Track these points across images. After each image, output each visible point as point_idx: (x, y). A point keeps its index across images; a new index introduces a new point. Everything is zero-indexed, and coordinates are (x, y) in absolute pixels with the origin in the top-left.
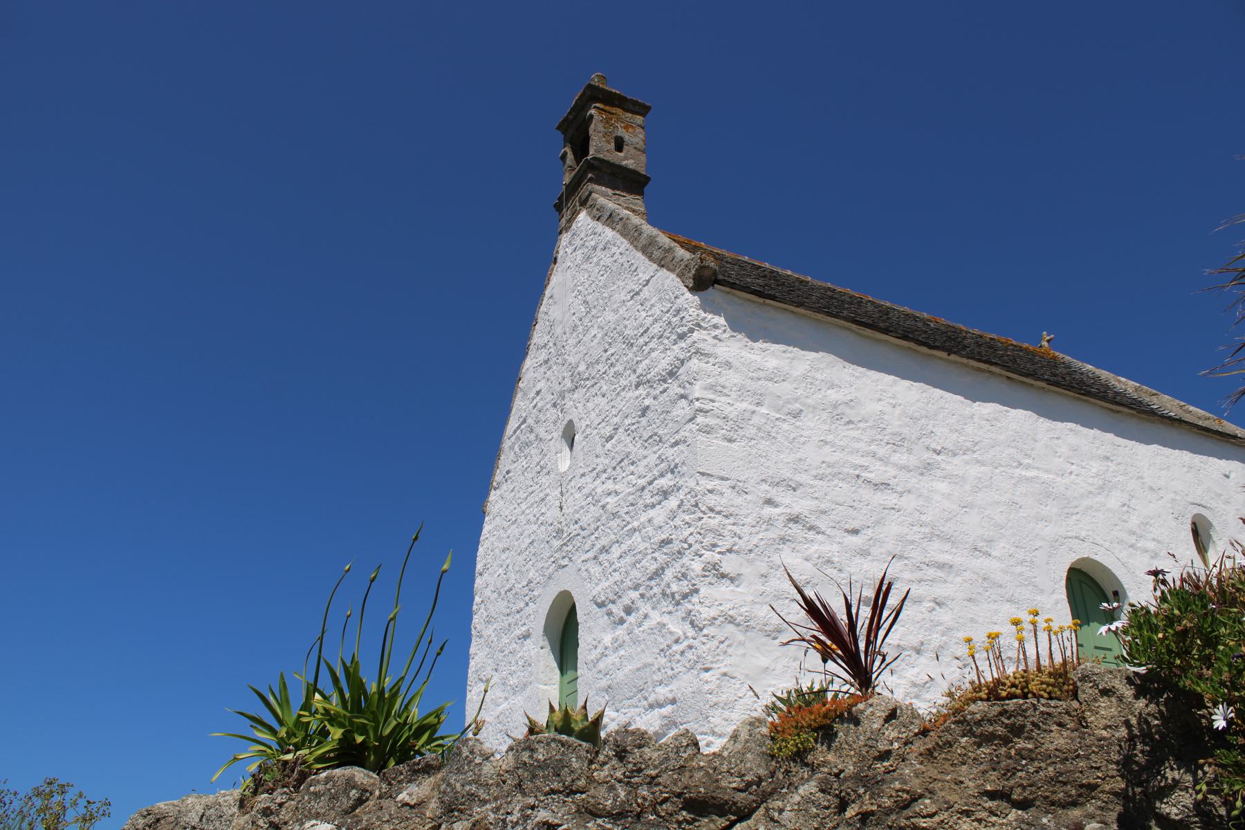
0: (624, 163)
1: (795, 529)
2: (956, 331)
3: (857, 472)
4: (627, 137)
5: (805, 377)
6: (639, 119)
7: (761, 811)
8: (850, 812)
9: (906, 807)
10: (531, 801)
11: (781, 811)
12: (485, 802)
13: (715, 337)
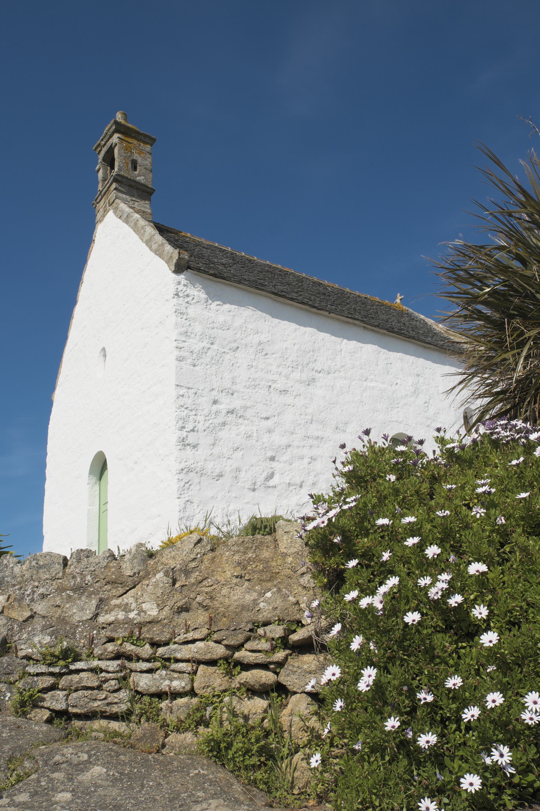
0: (138, 178)
1: (231, 418)
2: (343, 293)
3: (270, 384)
4: (139, 160)
5: (241, 327)
6: (148, 148)
7: (140, 585)
8: (177, 585)
9: (200, 582)
10: (36, 584)
11: (148, 585)
12: (14, 585)
13: (187, 302)
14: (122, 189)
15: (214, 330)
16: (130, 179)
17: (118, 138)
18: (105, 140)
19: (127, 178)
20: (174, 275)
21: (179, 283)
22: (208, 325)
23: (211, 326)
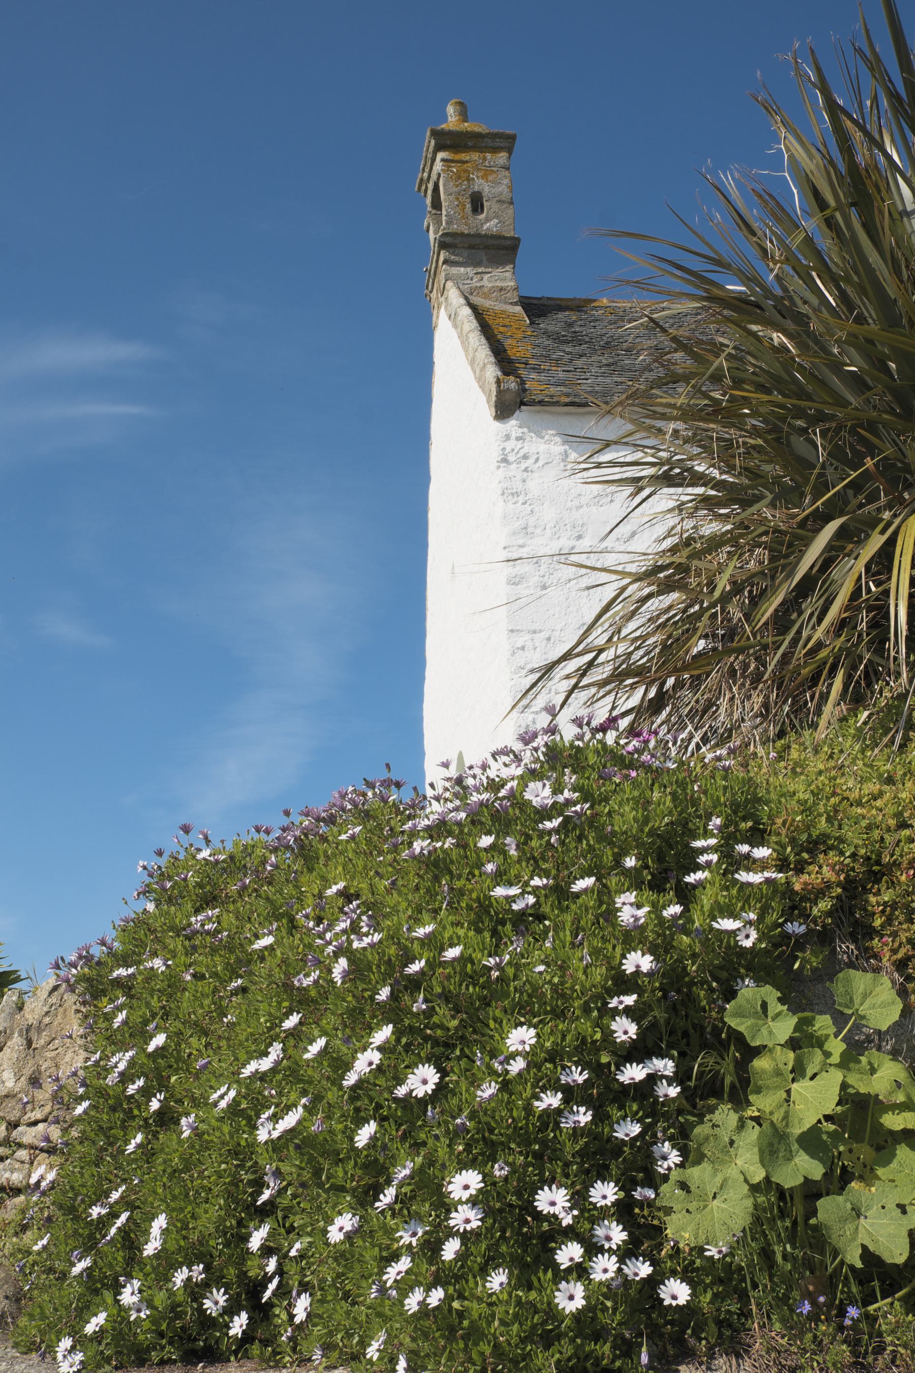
14: (457, 259)
15: (581, 511)
16: (468, 235)
17: (443, 160)
18: (427, 170)
19: (462, 234)
20: (497, 424)
21: (508, 437)
22: (569, 504)
23: (576, 503)
